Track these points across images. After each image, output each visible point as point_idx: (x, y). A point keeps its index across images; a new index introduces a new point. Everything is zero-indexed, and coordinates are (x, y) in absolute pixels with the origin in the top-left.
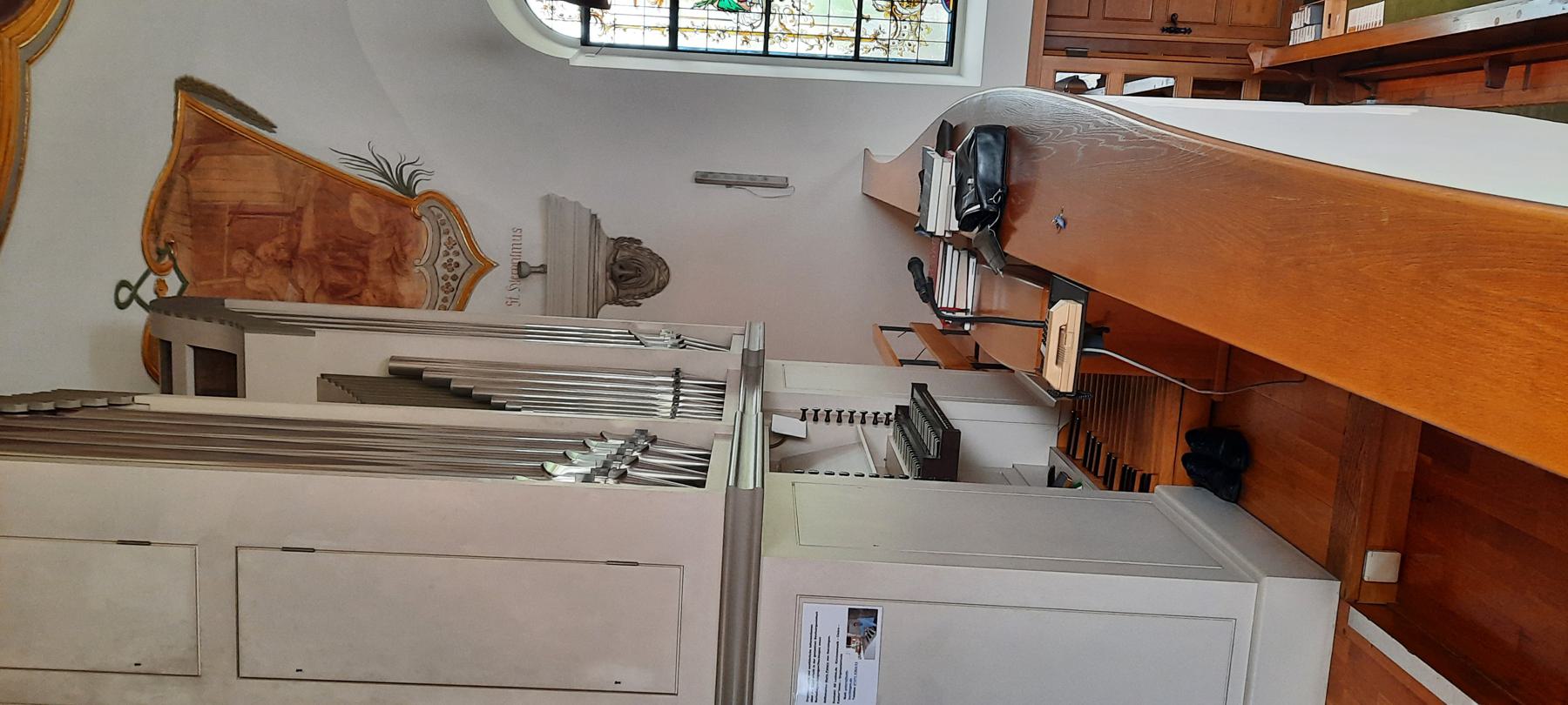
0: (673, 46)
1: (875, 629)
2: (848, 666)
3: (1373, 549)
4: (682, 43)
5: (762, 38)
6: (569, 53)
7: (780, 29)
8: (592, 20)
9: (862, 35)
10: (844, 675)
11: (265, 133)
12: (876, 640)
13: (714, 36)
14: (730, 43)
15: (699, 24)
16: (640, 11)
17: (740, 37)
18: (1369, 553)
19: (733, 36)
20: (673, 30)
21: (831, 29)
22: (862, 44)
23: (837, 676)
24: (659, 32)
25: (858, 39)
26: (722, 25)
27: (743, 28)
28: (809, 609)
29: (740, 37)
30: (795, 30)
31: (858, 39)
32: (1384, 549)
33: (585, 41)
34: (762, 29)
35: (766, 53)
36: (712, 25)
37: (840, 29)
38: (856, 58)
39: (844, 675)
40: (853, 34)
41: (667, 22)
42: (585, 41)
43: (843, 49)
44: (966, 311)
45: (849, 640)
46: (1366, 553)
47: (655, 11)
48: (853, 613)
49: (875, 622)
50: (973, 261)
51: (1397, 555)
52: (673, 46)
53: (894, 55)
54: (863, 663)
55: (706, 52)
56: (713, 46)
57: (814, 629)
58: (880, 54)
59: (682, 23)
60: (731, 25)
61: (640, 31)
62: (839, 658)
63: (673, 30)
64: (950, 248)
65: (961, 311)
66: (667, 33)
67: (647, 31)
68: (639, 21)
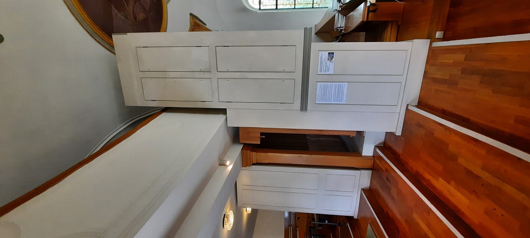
0: (277, 8)
1: (333, 56)
2: (328, 65)
3: (437, 31)
4: (278, 8)
5: (294, 5)
6: (258, 11)
7: (297, 3)
8: (261, 4)
9: (314, 3)
10: (327, 67)
11: (205, 26)
12: (334, 59)
13: (284, 5)
14: (288, 7)
15: (282, 3)
16: (270, 2)
17: (290, 5)
18: (437, 32)
19: (288, 5)
20: (277, 5)
21: (308, 2)
22: (314, 4)
23: (326, 66)
24: (274, 6)
25: (313, 4)
26: (286, 3)
27: (290, 3)
28: (321, 53)
29: (290, 5)
30: (300, 3)
31: (313, 4)
32: (440, 31)
33: (260, 9)
34: (294, 3)
35: (295, 8)
36: (284, 3)
37: (309, 2)
38: (313, 8)
39: (327, 67)
40: (312, 3)
41: (275, 3)
42: (260, 9)
43: (311, 6)
44: (343, 27)
45: (328, 59)
46: (436, 32)
47: (273, 2)
48: (329, 53)
49: (333, 55)
50: (344, 17)
51: (443, 32)
52: (277, 8)
53: (320, 6)
54: (331, 63)
55: (283, 9)
56: (284, 8)
57: (321, 58)
58: (318, 6)
59: (278, 3)
60: (288, 3)
61: (270, 6)
62: (326, 63)
63: (277, 5)
64: (340, 14)
65: (342, 27)
66: (275, 6)
67: (272, 6)
68: (270, 4)
